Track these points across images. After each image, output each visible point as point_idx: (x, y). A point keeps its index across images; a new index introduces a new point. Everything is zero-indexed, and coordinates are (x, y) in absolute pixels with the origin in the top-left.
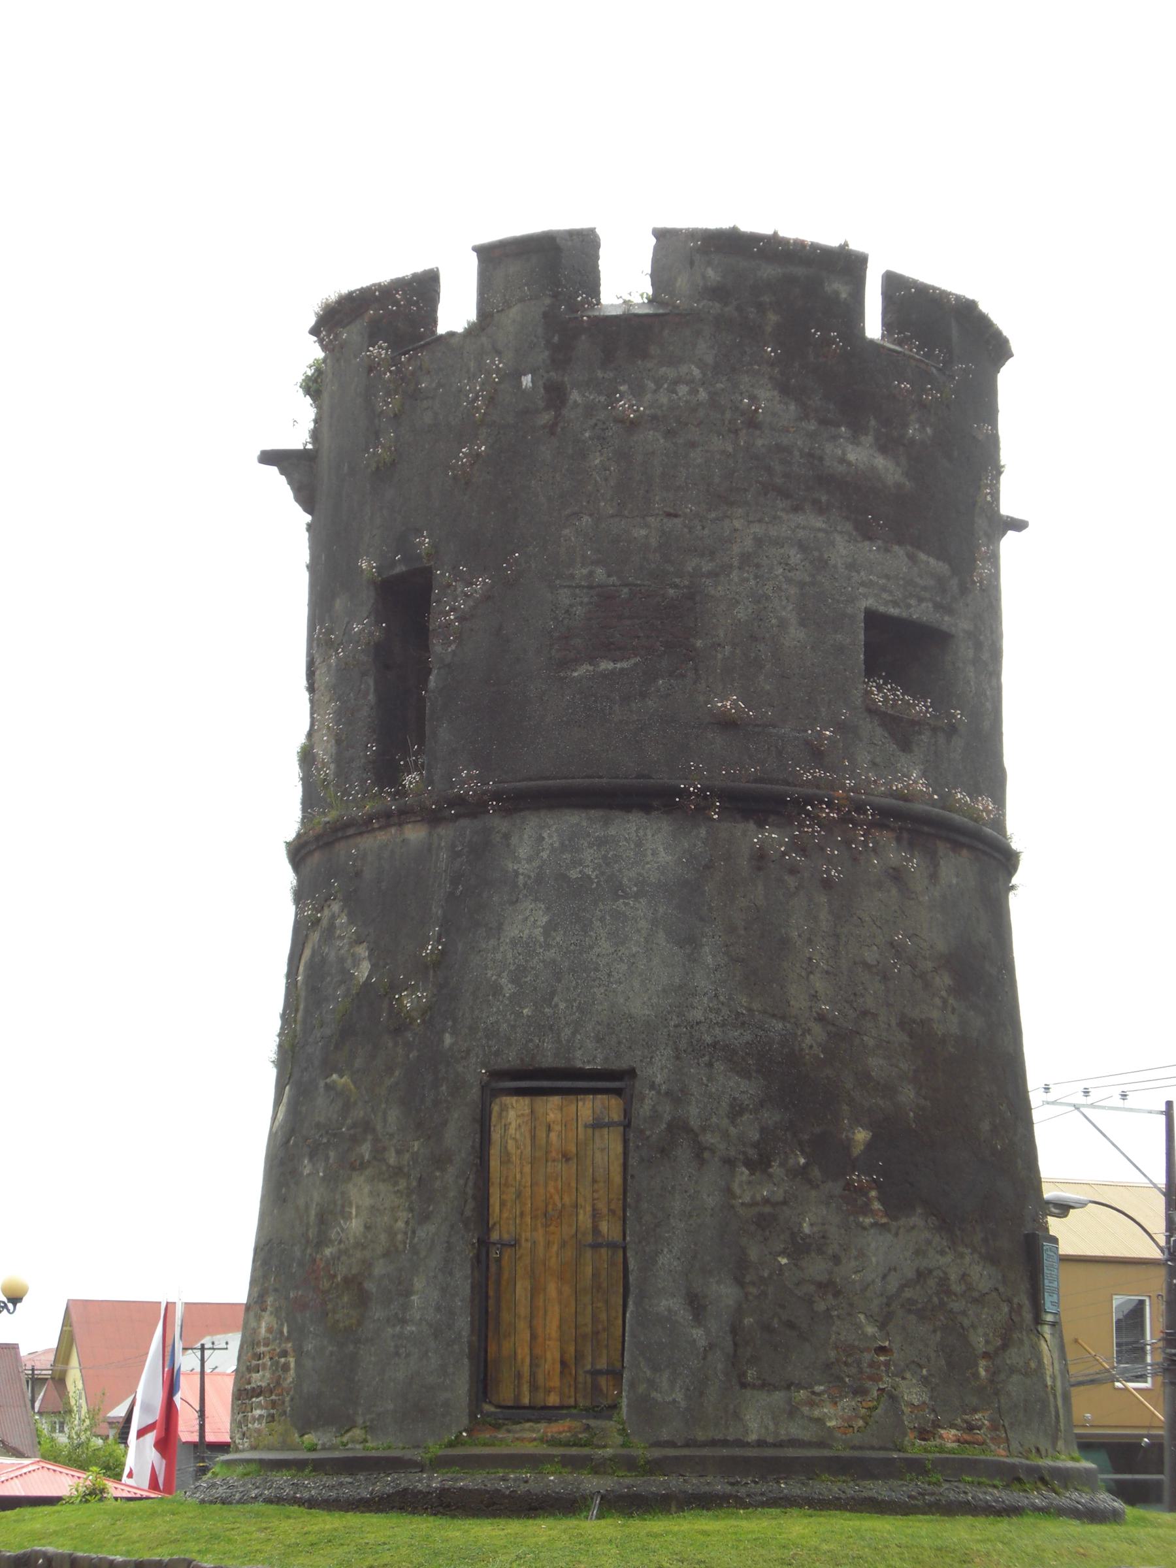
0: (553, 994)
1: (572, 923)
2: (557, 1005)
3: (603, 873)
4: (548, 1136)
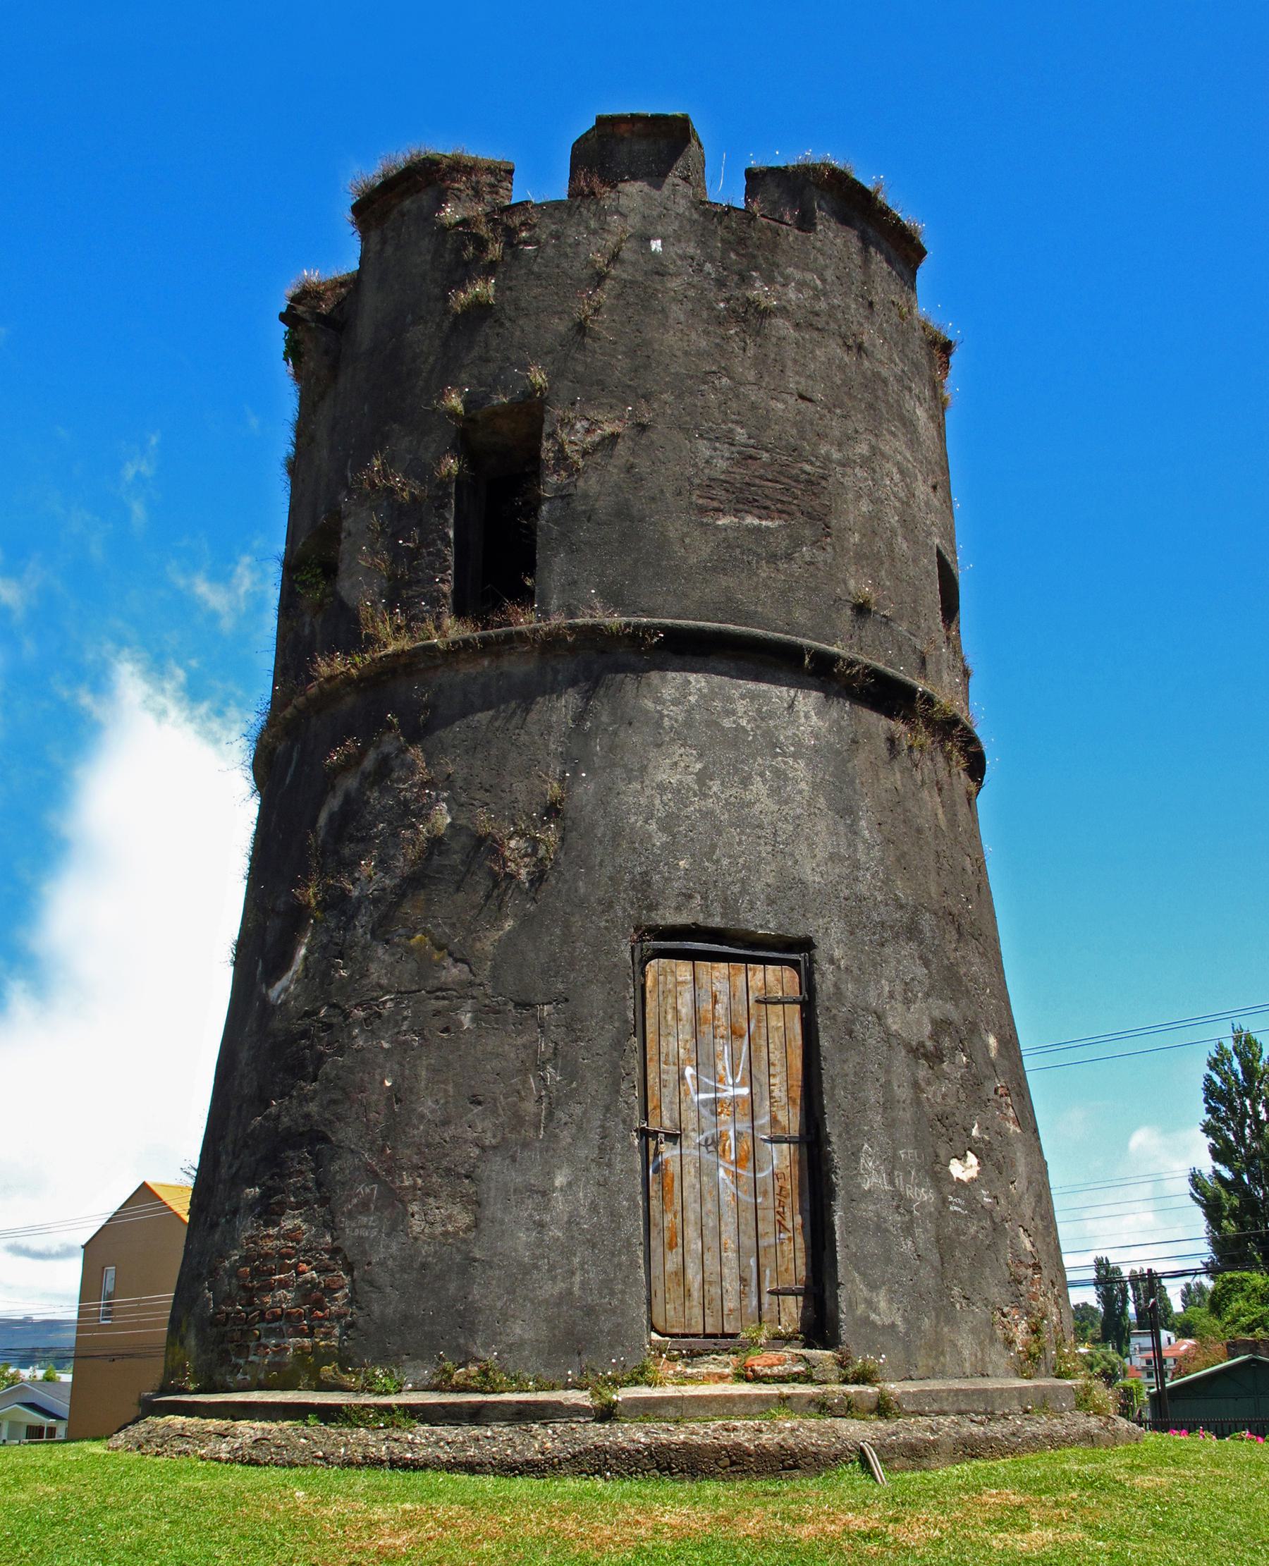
0: (714, 847)
1: (729, 773)
2: (718, 861)
3: (758, 727)
4: (714, 1008)
